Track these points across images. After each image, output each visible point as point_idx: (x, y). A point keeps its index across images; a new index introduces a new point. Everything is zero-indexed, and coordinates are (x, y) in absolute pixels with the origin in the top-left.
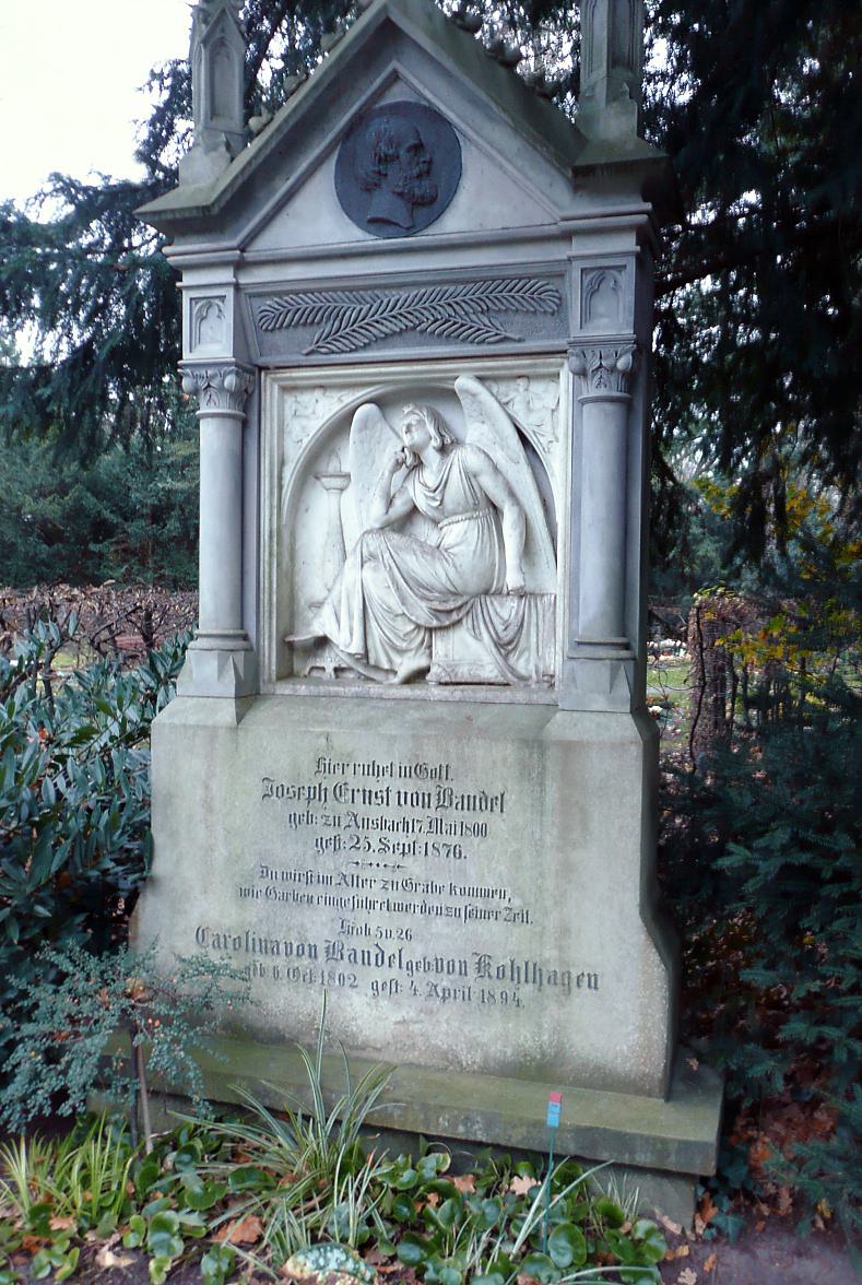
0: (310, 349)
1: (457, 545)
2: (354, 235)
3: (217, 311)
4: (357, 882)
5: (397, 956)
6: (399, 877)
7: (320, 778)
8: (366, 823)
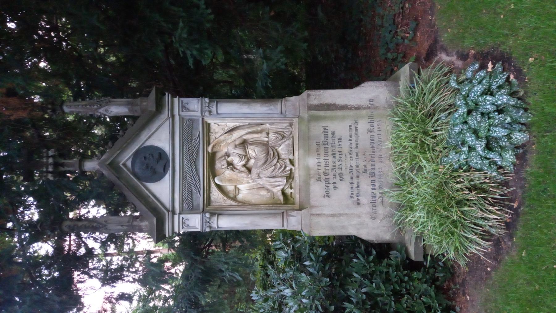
1: (255, 151)
2: (168, 177)
4: (351, 168)
6: (349, 156)
7: (322, 180)
8: (334, 166)
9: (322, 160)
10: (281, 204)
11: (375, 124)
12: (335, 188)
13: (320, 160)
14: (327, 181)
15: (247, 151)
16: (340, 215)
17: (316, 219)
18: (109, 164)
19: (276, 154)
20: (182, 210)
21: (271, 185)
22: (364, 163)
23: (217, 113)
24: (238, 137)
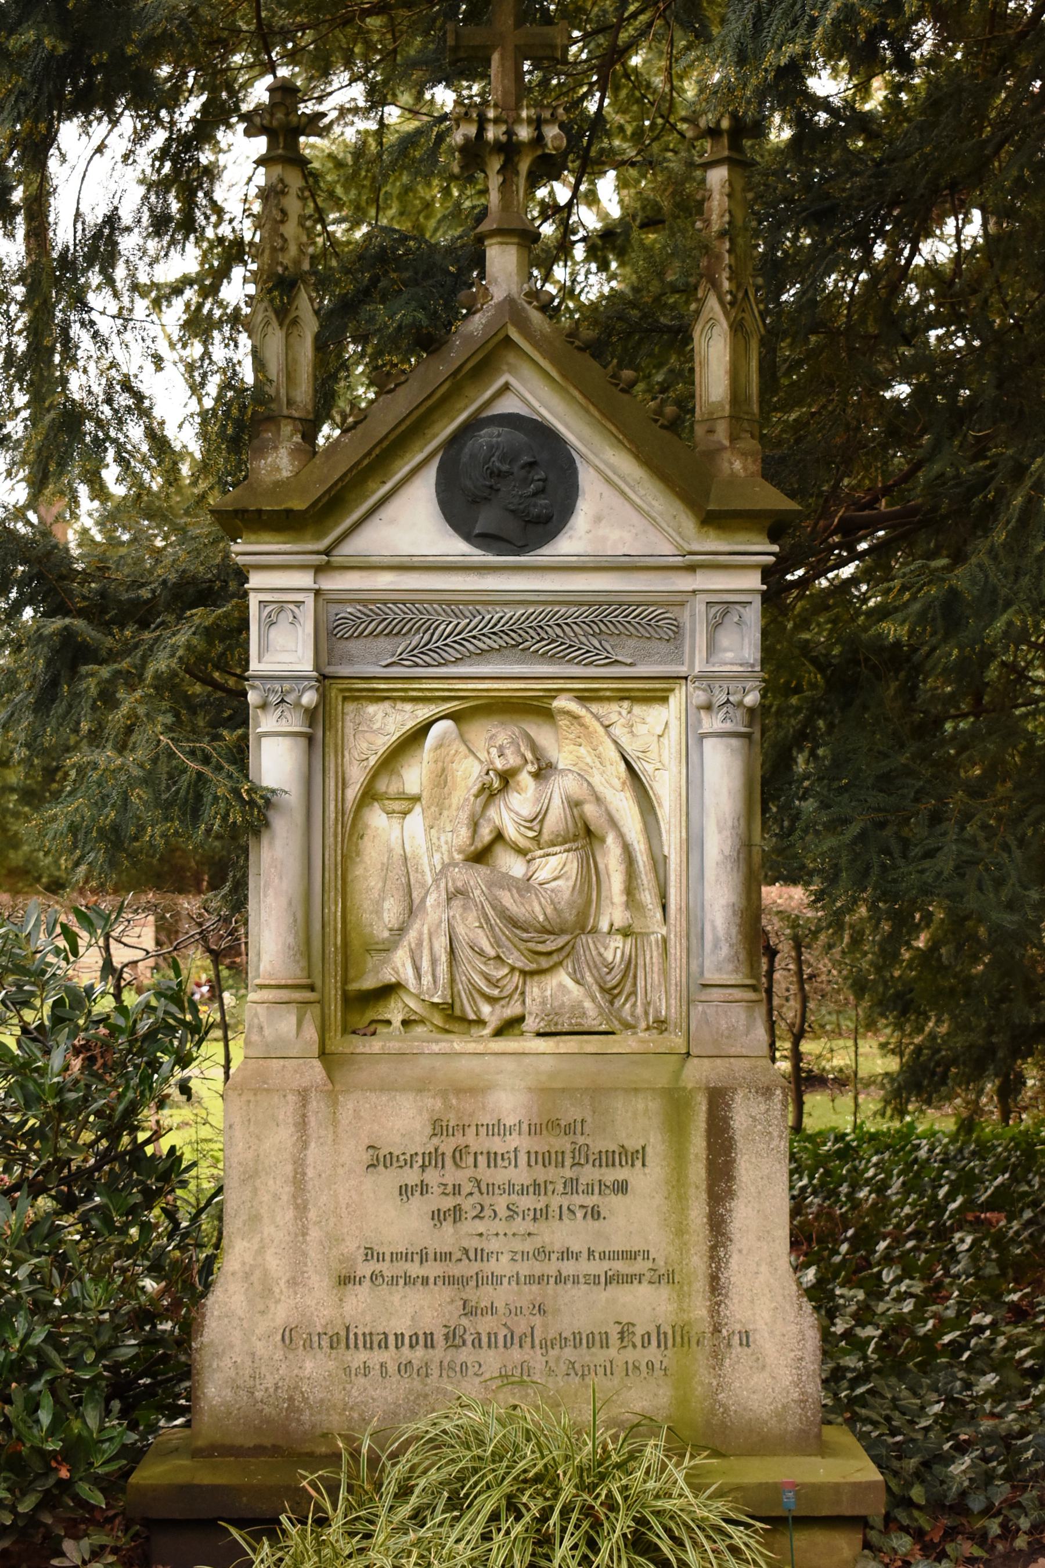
0: (389, 661)
1: (555, 879)
2: (457, 547)
3: (291, 619)
5: (529, 1334)
6: (528, 1246)
7: (435, 1141)
9: (514, 1141)
10: (345, 981)
11: (653, 1353)
12: (405, 1191)
13: (515, 1134)
14: (433, 1159)
15: (557, 849)
16: (301, 1209)
17: (286, 1110)
18: (508, 337)
19: (545, 963)
20: (329, 601)
21: (420, 944)
22: (500, 1304)
23: (703, 736)
24: (614, 812)
